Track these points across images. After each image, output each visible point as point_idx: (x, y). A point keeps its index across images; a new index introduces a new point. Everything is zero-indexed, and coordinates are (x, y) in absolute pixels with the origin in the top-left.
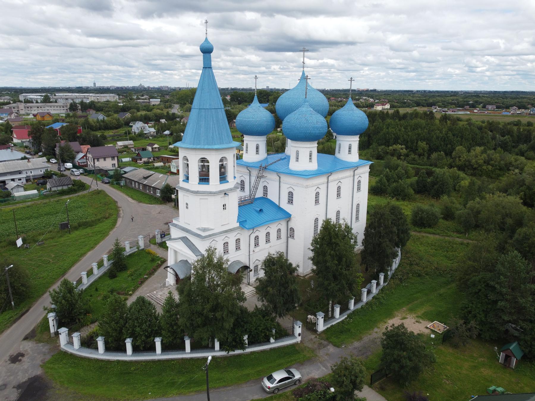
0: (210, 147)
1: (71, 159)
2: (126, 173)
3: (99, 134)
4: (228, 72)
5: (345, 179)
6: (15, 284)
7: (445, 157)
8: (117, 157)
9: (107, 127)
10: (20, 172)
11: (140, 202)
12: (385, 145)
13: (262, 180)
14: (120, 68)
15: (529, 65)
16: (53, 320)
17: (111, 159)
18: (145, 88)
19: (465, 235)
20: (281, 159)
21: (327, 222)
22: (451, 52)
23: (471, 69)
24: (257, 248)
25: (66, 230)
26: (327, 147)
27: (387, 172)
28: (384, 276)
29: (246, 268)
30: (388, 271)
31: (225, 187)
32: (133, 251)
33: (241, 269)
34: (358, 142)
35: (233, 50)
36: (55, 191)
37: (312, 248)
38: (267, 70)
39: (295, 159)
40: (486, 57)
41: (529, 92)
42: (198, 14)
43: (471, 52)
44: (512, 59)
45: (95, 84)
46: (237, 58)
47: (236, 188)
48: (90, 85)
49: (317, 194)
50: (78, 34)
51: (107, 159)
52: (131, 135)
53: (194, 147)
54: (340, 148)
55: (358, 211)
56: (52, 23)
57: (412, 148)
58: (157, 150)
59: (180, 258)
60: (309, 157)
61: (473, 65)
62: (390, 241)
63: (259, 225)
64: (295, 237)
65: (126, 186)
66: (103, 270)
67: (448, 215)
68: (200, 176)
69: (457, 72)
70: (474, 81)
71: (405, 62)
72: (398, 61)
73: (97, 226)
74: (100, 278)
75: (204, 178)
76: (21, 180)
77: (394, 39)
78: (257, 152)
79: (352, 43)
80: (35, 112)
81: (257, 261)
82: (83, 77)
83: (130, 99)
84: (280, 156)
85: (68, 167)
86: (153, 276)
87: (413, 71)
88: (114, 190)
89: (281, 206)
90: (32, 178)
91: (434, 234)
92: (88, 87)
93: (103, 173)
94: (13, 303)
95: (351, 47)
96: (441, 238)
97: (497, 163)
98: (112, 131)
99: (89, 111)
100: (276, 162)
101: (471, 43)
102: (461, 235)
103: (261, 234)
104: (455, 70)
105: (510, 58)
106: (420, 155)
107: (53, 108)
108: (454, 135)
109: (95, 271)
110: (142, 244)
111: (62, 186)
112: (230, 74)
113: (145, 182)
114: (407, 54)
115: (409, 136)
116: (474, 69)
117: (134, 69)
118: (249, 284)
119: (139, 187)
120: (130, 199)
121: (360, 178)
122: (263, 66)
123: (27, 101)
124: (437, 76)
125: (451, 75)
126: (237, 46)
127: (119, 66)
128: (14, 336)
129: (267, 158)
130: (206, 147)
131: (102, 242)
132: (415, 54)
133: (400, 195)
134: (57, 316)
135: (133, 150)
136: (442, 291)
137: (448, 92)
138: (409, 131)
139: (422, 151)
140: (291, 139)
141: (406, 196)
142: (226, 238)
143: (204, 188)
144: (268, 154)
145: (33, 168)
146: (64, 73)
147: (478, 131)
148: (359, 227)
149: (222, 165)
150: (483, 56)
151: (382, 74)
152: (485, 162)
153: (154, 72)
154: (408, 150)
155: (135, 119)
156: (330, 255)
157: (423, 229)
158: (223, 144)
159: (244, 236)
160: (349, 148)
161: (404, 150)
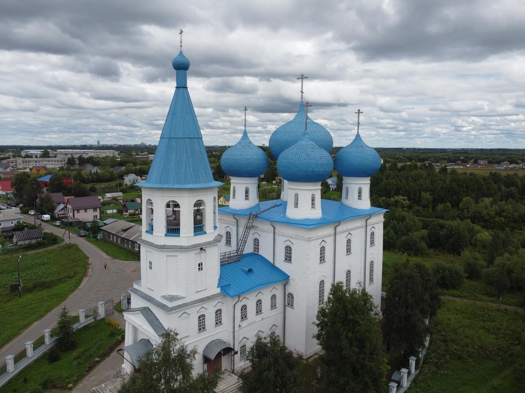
0: (181, 186)
1: (51, 210)
2: (106, 224)
3: (89, 186)
4: (227, 132)
5: (356, 231)
7: (451, 209)
8: (100, 208)
9: (99, 179)
11: (115, 257)
12: (386, 197)
13: (252, 231)
14: (124, 128)
15: (513, 124)
17: (92, 210)
18: (147, 146)
19: (499, 298)
20: (276, 206)
21: (336, 289)
22: (438, 113)
23: (458, 128)
24: (245, 321)
25: (16, 293)
26: (332, 194)
27: (394, 224)
28: (416, 361)
29: (228, 351)
30: (418, 352)
31: (201, 239)
32: (89, 322)
33: (222, 352)
34: (369, 185)
35: (231, 111)
36: (22, 245)
37: (317, 322)
38: (263, 130)
39: (293, 205)
40: (472, 117)
41: (514, 150)
42: (200, 79)
43: (457, 113)
44: (496, 120)
45: (99, 142)
46: (235, 119)
47: (217, 240)
48: (94, 143)
49: (323, 249)
50: (87, 97)
51: (88, 210)
52: (121, 187)
53: (161, 186)
54: (347, 192)
55: (372, 271)
56: (63, 87)
57: (415, 199)
59: (140, 337)
60: (310, 202)
61: (459, 125)
62: (421, 312)
63: (248, 291)
64: (294, 306)
65: (104, 240)
66: (42, 350)
67: (473, 273)
68: (168, 225)
69: (444, 131)
70: (461, 139)
71: (395, 122)
72: (388, 121)
73: (56, 287)
74: (36, 362)
75: (173, 228)
77: (384, 101)
78: (247, 197)
79: (344, 105)
80: (31, 167)
81: (245, 340)
82: (89, 136)
83: (130, 155)
84: (275, 202)
85: (45, 219)
86: (108, 359)
87: (402, 131)
88: (89, 244)
89: (277, 265)
91: (460, 297)
92: (92, 145)
93: (81, 225)
95: (343, 108)
96: (471, 302)
97: (510, 215)
98: (104, 184)
99: (86, 165)
100: (269, 209)
101: (457, 105)
102: (493, 299)
104: (442, 130)
105: (494, 118)
106: (424, 207)
107: (51, 163)
108: (459, 186)
109: (30, 352)
110: (102, 313)
111: (30, 239)
112: (228, 133)
113: (124, 235)
114: (396, 114)
115: (411, 186)
116: (461, 128)
117: (137, 129)
118: (233, 372)
119: (117, 241)
120: (104, 255)
121: (373, 229)
122: (260, 126)
123: (27, 156)
124: (425, 135)
125: (438, 134)
126: (235, 107)
127: (124, 126)
129: (258, 205)
130: (176, 186)
131: (56, 309)
132: (404, 115)
135: (121, 201)
136: (496, 382)
137: (436, 149)
138: (410, 182)
139: (426, 202)
140: (288, 180)
142: (203, 310)
143: (172, 241)
144: (260, 201)
145: (3, 219)
146: (71, 132)
147: (483, 182)
148: (375, 290)
149: (198, 210)
150: (469, 116)
151: (373, 133)
152: (496, 214)
153: (156, 132)
154: (411, 202)
155: (127, 173)
156: (347, 338)
158: (200, 183)
160: (358, 193)
161: (407, 201)
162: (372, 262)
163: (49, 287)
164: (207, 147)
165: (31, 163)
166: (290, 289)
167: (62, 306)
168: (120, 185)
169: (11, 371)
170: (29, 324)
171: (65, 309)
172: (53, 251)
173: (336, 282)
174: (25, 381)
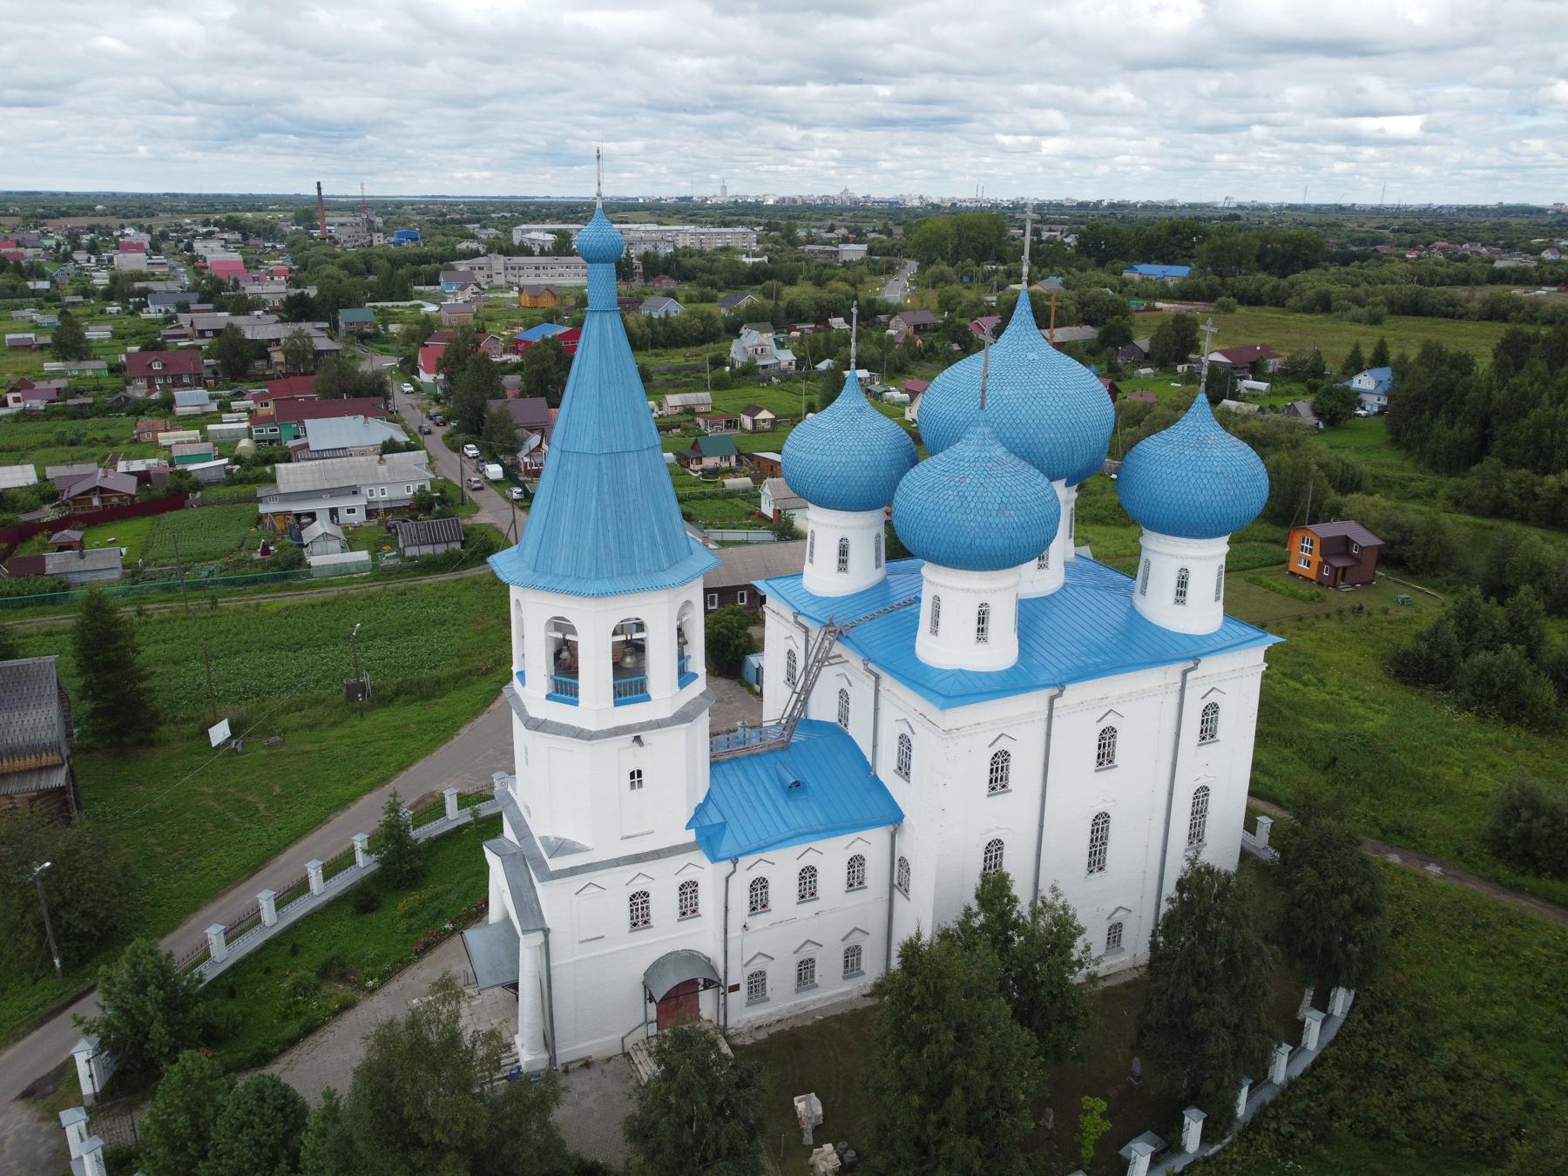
5: (1140, 700)
10: (355, 491)
16: (88, 1061)
36: (413, 558)
45: (724, 188)
58: (767, 426)
60: (974, 625)
66: (344, 881)
73: (441, 701)
76: (353, 511)
78: (843, 563)
85: (492, 477)
94: (57, 962)
98: (683, 350)
103: (781, 867)
109: (316, 883)
133: (1496, 699)
134: (103, 1045)
141: (1521, 706)
157: (1529, 881)
159: (708, 874)
162: (1204, 790)
163: (427, 697)
166: (903, 849)
167: (388, 789)
168: (718, 362)
169: (268, 924)
170: (354, 799)
171: (394, 795)
172: (476, 583)
173: (559, 1062)
174: (295, 951)
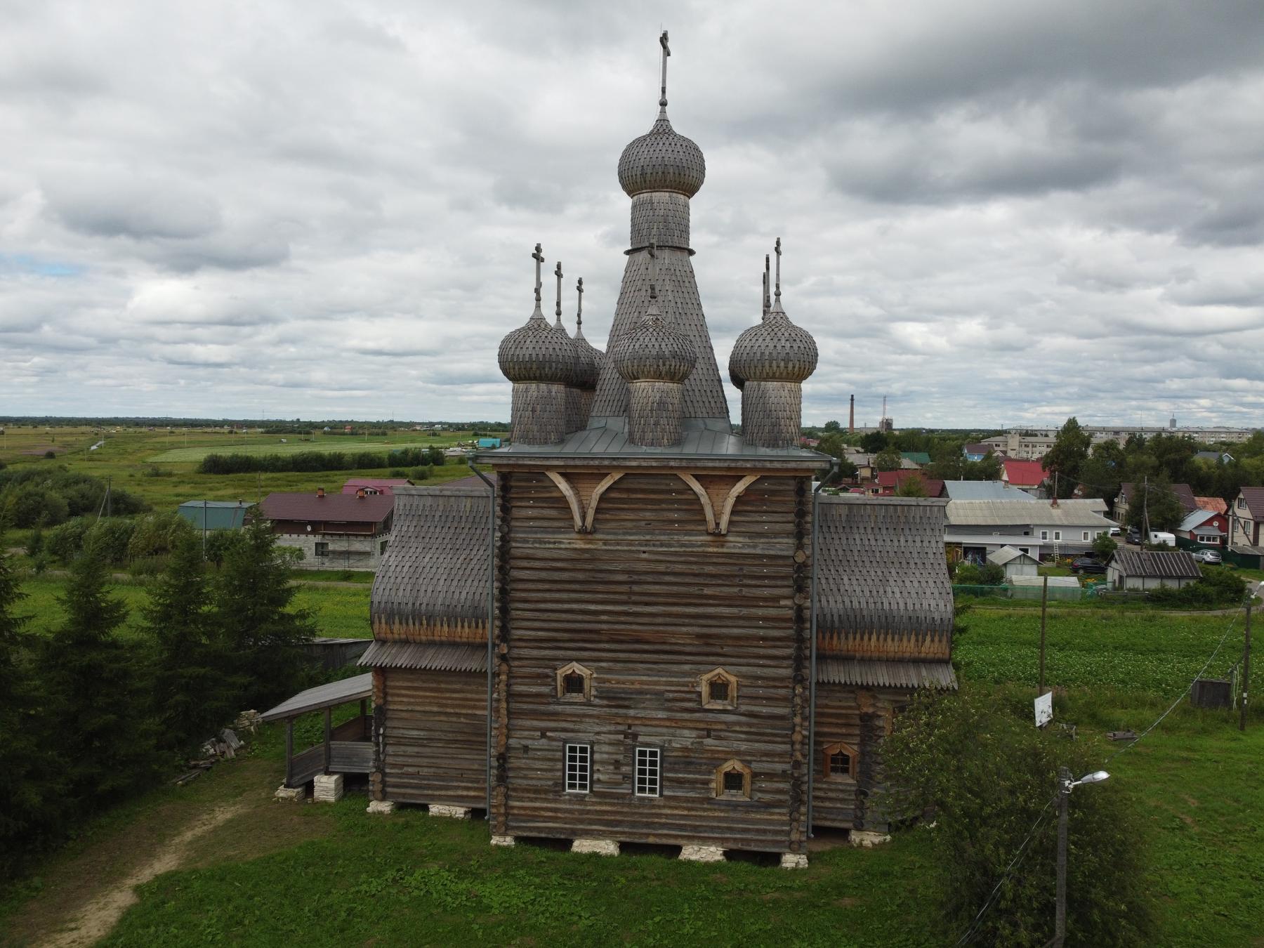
6: (1097, 893)
10: (1026, 530)
36: (1136, 590)
45: (1173, 422)
90: (1057, 552)
111: (1162, 577)
128: (448, 54)
145: (1066, 523)
164: (312, 781)
165: (1038, 449)
